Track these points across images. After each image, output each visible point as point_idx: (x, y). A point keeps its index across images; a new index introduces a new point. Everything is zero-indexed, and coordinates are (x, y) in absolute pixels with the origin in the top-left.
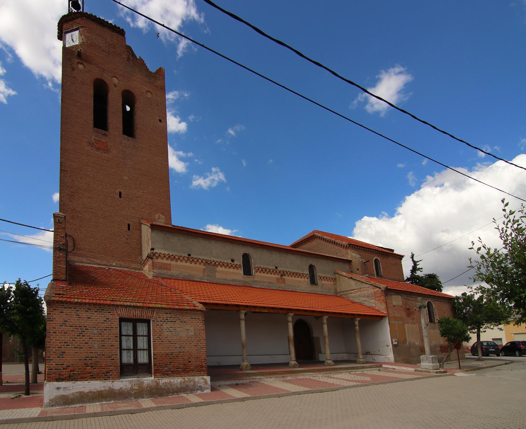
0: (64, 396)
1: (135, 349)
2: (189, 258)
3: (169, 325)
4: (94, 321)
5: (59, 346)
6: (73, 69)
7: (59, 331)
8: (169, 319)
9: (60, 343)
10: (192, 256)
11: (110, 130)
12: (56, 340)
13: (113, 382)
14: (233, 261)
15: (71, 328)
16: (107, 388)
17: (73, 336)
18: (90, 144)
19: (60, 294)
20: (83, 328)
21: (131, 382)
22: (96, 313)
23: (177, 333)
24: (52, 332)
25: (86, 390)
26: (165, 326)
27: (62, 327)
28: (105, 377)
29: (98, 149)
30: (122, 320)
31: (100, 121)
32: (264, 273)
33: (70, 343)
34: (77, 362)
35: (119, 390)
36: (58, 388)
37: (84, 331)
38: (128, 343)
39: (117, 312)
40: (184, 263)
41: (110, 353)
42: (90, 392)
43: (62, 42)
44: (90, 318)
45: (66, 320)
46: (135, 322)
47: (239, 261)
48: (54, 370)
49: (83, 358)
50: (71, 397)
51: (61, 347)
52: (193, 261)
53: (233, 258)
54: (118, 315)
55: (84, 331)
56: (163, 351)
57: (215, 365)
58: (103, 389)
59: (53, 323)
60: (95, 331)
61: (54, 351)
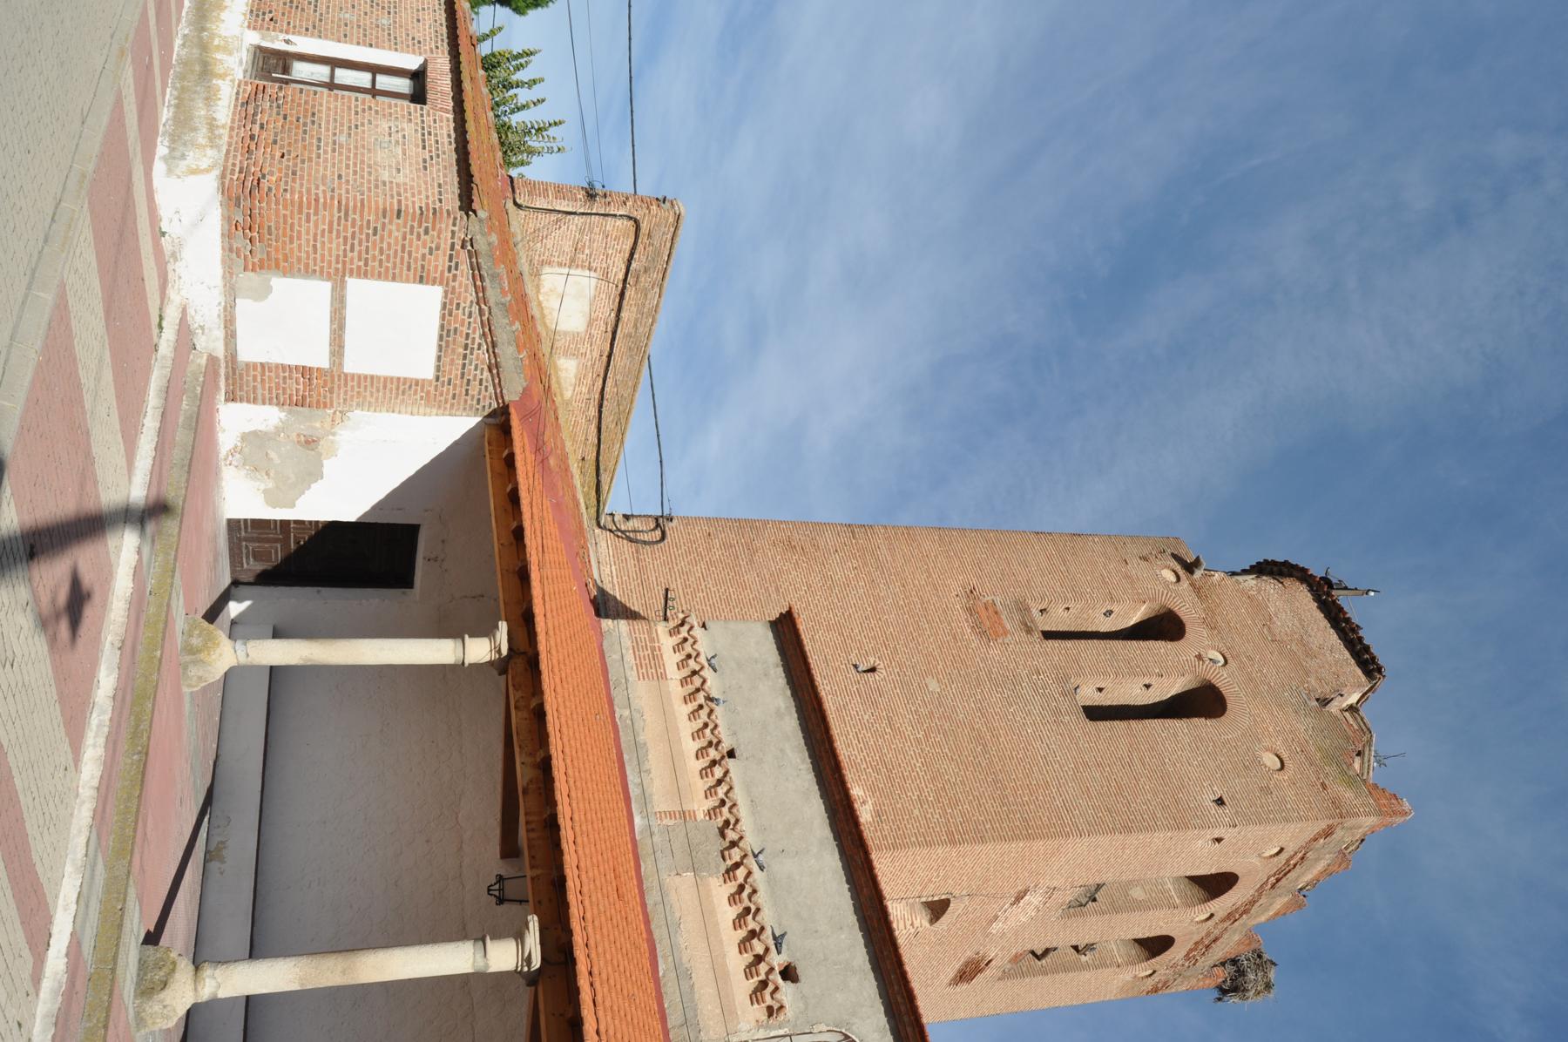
2: (719, 757)
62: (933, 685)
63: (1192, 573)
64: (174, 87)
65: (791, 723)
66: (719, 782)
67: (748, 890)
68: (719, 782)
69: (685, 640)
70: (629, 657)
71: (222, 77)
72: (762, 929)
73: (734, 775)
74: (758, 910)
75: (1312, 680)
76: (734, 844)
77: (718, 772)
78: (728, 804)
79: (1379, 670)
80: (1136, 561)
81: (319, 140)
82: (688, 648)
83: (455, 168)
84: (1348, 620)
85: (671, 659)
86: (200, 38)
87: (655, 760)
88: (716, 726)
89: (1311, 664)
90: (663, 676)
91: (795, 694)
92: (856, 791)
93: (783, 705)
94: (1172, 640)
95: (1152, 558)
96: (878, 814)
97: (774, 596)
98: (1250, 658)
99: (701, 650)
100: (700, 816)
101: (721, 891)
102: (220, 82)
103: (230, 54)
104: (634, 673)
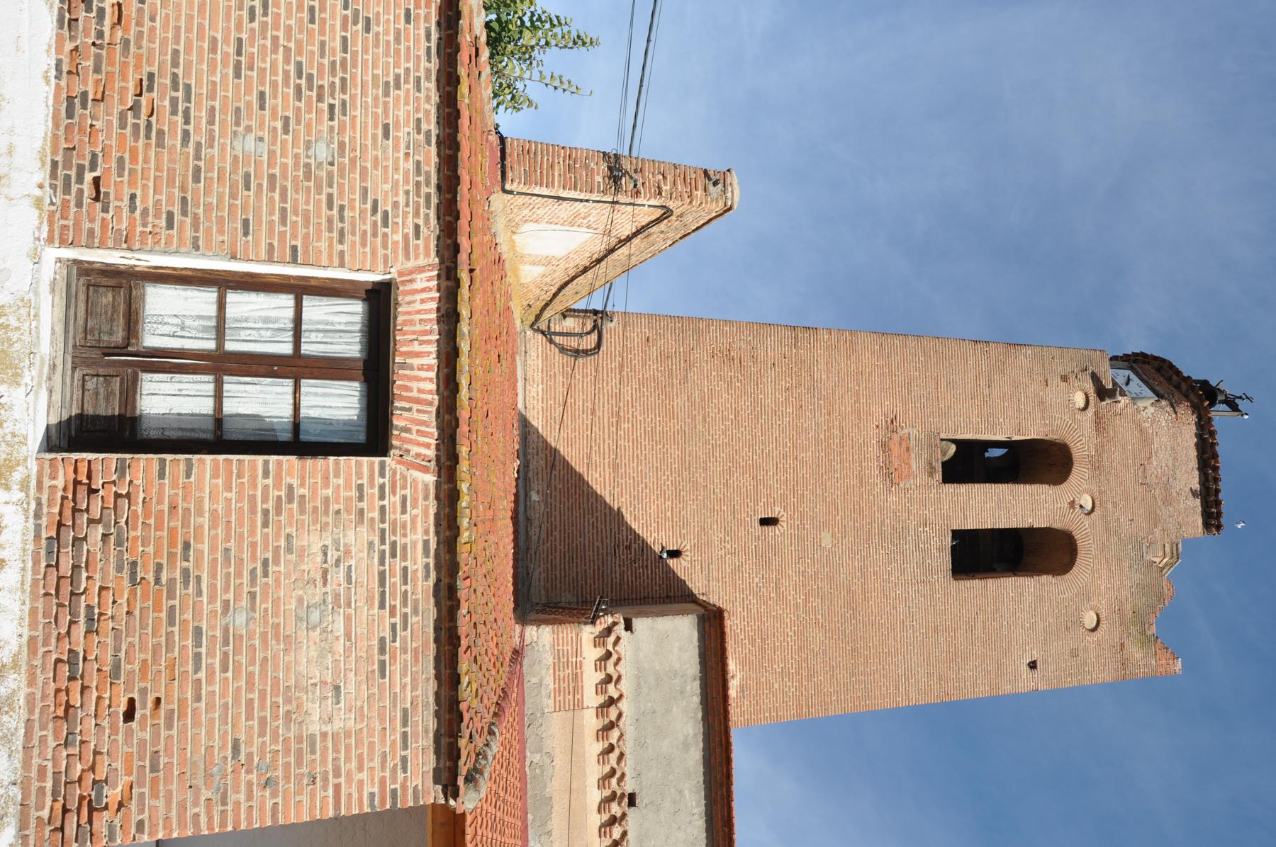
1: (223, 364)
3: (364, 565)
4: (371, 154)
6: (1064, 378)
8: (398, 564)
10: (631, 812)
11: (951, 488)
13: (38, 203)
15: (338, 44)
17: (299, 43)
21: (28, 306)
22: (410, 165)
23: (315, 616)
26: (358, 538)
28: (67, 165)
29: (884, 446)
30: (379, 301)
31: (969, 463)
33: (264, 26)
34: (164, 42)
37: (320, 98)
38: (259, 322)
39: (421, 270)
40: (594, 771)
41: (208, 208)
44: (386, 135)
45: (374, 28)
46: (375, 370)
49: (187, 72)
55: (320, 98)
56: (205, 521)
57: (157, 376)
60: (322, 152)
62: (827, 541)
63: (1102, 399)
65: (695, 755)
70: (549, 680)
72: (621, 696)
74: (619, 659)
75: (1157, 531)
77: (615, 809)
79: (1219, 527)
80: (1055, 381)
83: (432, 707)
84: (1216, 469)
88: (619, 659)
89: (1164, 512)
90: (578, 705)
91: (705, 718)
92: (732, 665)
93: (691, 732)
94: (1055, 484)
95: (1072, 377)
96: (742, 689)
97: (700, 427)
98: (1115, 504)
99: (623, 672)
103: (15, 381)
104: (551, 702)
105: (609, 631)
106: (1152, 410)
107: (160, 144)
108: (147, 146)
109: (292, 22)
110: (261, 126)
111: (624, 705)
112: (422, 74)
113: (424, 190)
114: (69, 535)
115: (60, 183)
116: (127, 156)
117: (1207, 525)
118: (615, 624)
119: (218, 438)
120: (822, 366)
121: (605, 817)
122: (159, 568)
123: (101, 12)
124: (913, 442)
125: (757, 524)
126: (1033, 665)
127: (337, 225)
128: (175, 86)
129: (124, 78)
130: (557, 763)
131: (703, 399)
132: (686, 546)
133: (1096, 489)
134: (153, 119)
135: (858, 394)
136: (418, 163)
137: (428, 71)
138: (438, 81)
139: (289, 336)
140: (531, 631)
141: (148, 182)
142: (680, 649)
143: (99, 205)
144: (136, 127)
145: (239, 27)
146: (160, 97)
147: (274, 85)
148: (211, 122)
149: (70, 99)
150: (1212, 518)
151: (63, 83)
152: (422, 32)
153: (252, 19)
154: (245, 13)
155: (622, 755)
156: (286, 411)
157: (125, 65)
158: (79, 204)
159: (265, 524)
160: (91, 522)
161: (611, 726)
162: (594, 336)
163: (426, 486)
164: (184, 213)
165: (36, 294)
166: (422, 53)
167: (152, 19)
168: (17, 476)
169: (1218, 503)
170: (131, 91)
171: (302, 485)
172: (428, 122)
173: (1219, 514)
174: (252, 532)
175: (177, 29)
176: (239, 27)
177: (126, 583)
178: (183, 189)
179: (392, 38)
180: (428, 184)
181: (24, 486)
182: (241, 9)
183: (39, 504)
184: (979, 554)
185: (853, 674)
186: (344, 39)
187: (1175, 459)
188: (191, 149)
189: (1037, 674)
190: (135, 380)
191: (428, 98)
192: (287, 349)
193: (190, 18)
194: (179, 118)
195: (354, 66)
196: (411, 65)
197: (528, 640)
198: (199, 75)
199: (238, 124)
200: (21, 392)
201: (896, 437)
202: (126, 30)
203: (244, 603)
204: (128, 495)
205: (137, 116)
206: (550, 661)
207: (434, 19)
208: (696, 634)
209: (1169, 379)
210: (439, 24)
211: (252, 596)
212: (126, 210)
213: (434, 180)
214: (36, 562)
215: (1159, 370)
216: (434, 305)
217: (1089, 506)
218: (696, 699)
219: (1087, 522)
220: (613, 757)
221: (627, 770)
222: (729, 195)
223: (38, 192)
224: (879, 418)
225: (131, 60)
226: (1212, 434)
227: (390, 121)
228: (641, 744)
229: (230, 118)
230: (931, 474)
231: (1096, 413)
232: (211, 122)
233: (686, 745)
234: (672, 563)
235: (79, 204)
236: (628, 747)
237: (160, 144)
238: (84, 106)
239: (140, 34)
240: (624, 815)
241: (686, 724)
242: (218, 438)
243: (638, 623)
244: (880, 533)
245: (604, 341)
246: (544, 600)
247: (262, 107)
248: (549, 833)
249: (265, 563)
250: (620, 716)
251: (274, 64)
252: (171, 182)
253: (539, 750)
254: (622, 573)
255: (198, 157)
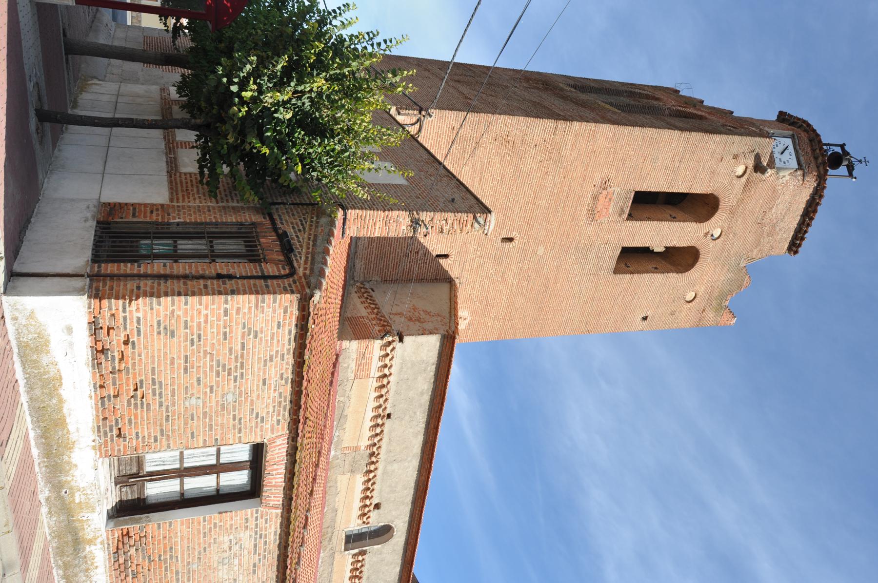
0: (47, 343)
2: (382, 416)
5: (190, 324)
6: (735, 157)
7: (231, 321)
9: (199, 324)
11: (630, 223)
12: (207, 316)
13: (94, 448)
14: (377, 506)
16: (73, 437)
18: (605, 184)
19: (315, 241)
20: (239, 371)
22: (277, 394)
24: (228, 306)
25: (65, 392)
27: (241, 326)
28: (105, 425)
29: (595, 198)
30: (258, 451)
31: (646, 203)
32: (352, 571)
33: (199, 346)
35: (69, 463)
36: (69, 330)
37: (229, 374)
41: (173, 431)
42: (61, 401)
43: (775, 118)
45: (259, 335)
47: (376, 520)
48: (122, 314)
50: (45, 360)
51: (186, 328)
52: (377, 426)
53: (382, 507)
54: (272, 440)
55: (229, 374)
58: (71, 427)
59: (250, 308)
60: (230, 398)
61: (177, 313)
62: (541, 251)
64: (58, 567)
65: (426, 399)
66: (377, 435)
67: (391, 347)
68: (377, 435)
69: (375, 444)
71: (90, 542)
72: (391, 374)
73: (386, 429)
74: (393, 358)
75: (755, 251)
76: (373, 463)
77: (379, 421)
78: (384, 398)
79: (796, 252)
81: (177, 572)
82: (387, 361)
84: (812, 219)
85: (376, 363)
86: (61, 498)
87: (349, 425)
88: (393, 358)
89: (765, 240)
98: (735, 235)
100: (363, 448)
101: (360, 479)
102: (93, 548)
103: (93, 511)
105: (390, 343)
106: (788, 178)
107: (148, 409)
108: (142, 411)
109: (214, 341)
110: (199, 392)
111: (391, 379)
112: (285, 352)
113: (283, 404)
114: (121, 552)
115: (102, 434)
116: (133, 417)
117: (790, 249)
118: (393, 341)
119: (184, 502)
120: (569, 147)
121: (380, 374)
122: (160, 556)
123: (113, 357)
124: (615, 196)
125: (499, 241)
126: (645, 318)
127: (238, 426)
128: (154, 383)
129: (128, 385)
130: (352, 401)
131: (482, 167)
132: (453, 253)
133: (726, 226)
134: (144, 400)
135: (588, 165)
136: (281, 393)
137: (289, 350)
138: (294, 353)
139: (215, 457)
140: (346, 344)
141: (142, 426)
142: (428, 351)
143: (121, 439)
144: (136, 404)
145: (186, 350)
146: (147, 389)
147: (205, 373)
148: (173, 395)
149: (102, 398)
150: (794, 246)
151: (98, 393)
152: (287, 332)
153: (192, 344)
154: (189, 343)
155: (386, 400)
156: (215, 484)
157: (128, 379)
158: (112, 440)
159: (204, 537)
160: (130, 546)
161: (383, 386)
162: (417, 126)
163: (277, 515)
164: (162, 435)
165: (98, 481)
166: (286, 341)
167: (140, 355)
168: (99, 540)
169: (802, 239)
170: (132, 388)
171: (221, 521)
172: (287, 373)
173: (800, 245)
174: (199, 539)
175: (153, 357)
176: (186, 350)
177: (147, 561)
178: (161, 425)
179: (269, 338)
180: (285, 401)
181: (102, 543)
182: (186, 341)
183: (109, 544)
184: (633, 258)
185: (536, 320)
186: (243, 344)
187: (789, 209)
188: (164, 408)
189: (645, 323)
190: (144, 485)
191: (287, 363)
192: (214, 462)
193: (159, 350)
194: (157, 397)
195: (248, 355)
196: (279, 349)
197: (344, 347)
198: (165, 377)
199: (187, 393)
200: (97, 514)
201: (605, 192)
202: (127, 363)
203: (196, 560)
204: (145, 536)
205: (136, 399)
206: (355, 357)
207: (294, 323)
208: (438, 344)
209: (813, 150)
210: (296, 325)
211: (200, 558)
212: (134, 438)
213: (289, 398)
214: (110, 562)
215: (811, 141)
216: (285, 450)
217: (716, 236)
218: (432, 374)
219: (712, 244)
220: (382, 400)
221: (388, 406)
222: (487, 228)
223: (93, 444)
224: (598, 179)
225: (131, 376)
226: (821, 197)
227: (267, 377)
228: (397, 393)
229: (183, 391)
230: (620, 215)
231: (748, 179)
232: (173, 395)
233: (422, 393)
234: (442, 261)
235: (112, 440)
236: (390, 396)
237: (148, 409)
238: (109, 400)
239: (134, 364)
240: (383, 424)
241: (425, 385)
242: (184, 502)
243: (406, 339)
244: (576, 248)
245: (423, 130)
246: (362, 279)
247: (199, 384)
248: (344, 429)
249: (205, 549)
250: (389, 383)
251: (205, 364)
252: (155, 423)
253: (343, 396)
254: (410, 267)
255: (167, 411)
